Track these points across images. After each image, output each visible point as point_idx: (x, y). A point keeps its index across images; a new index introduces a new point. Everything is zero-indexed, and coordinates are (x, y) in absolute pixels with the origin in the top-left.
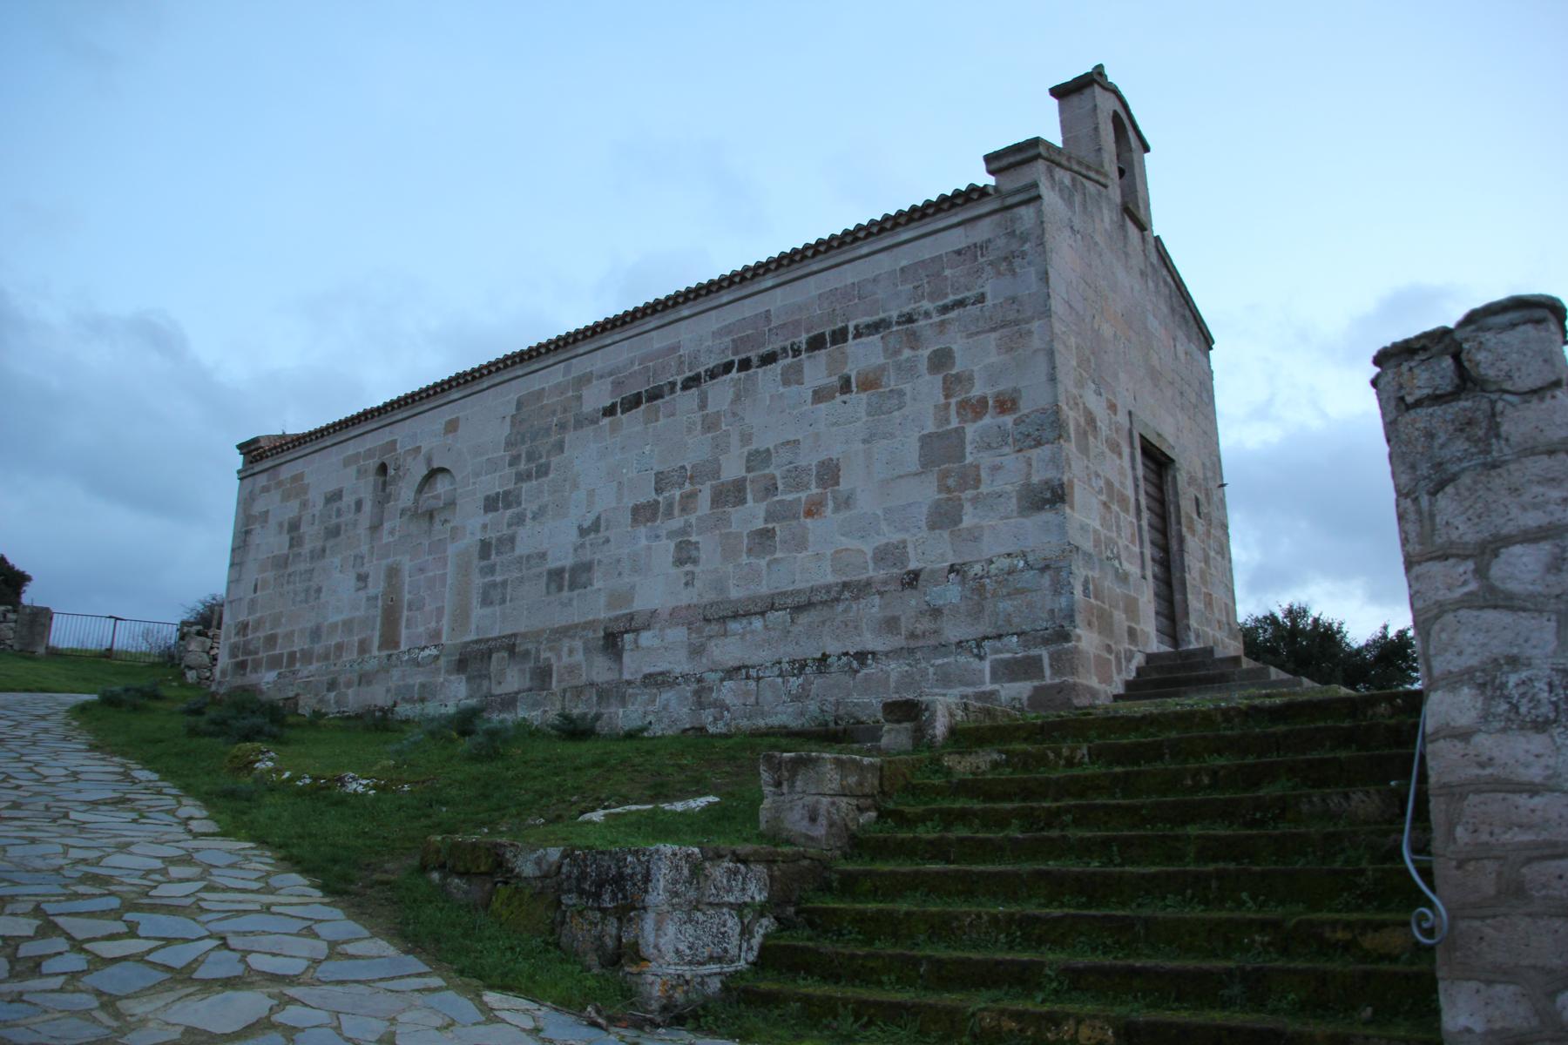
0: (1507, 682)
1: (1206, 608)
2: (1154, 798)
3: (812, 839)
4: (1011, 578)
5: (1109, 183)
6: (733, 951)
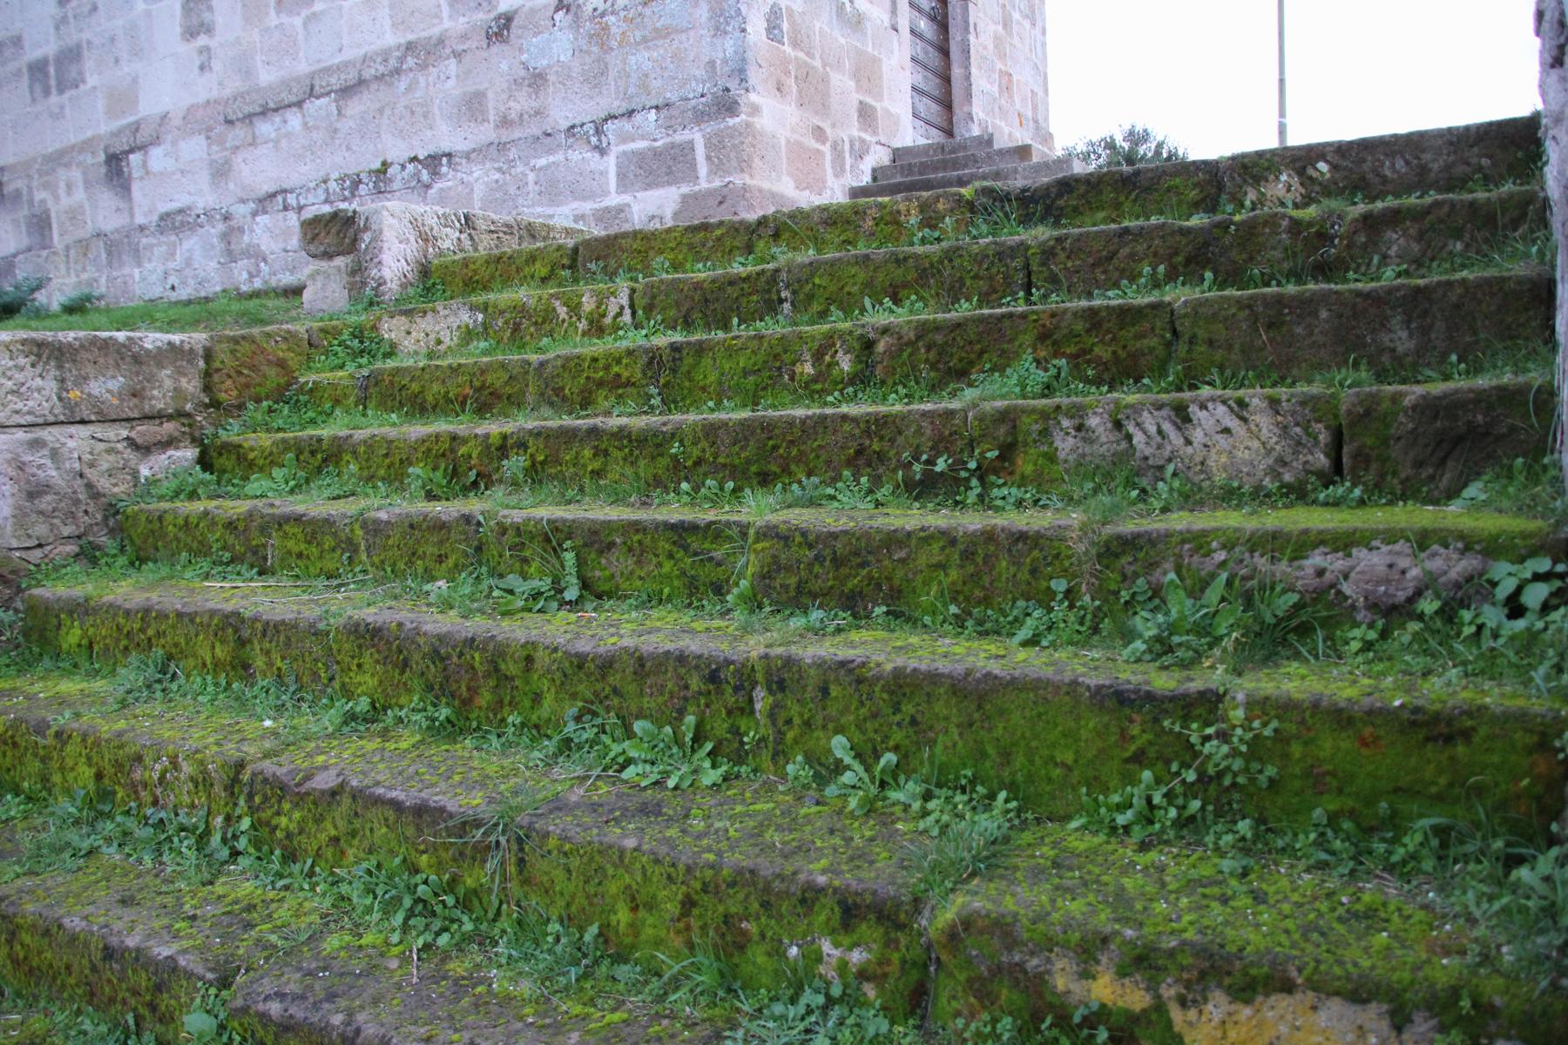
1: (1001, 92)
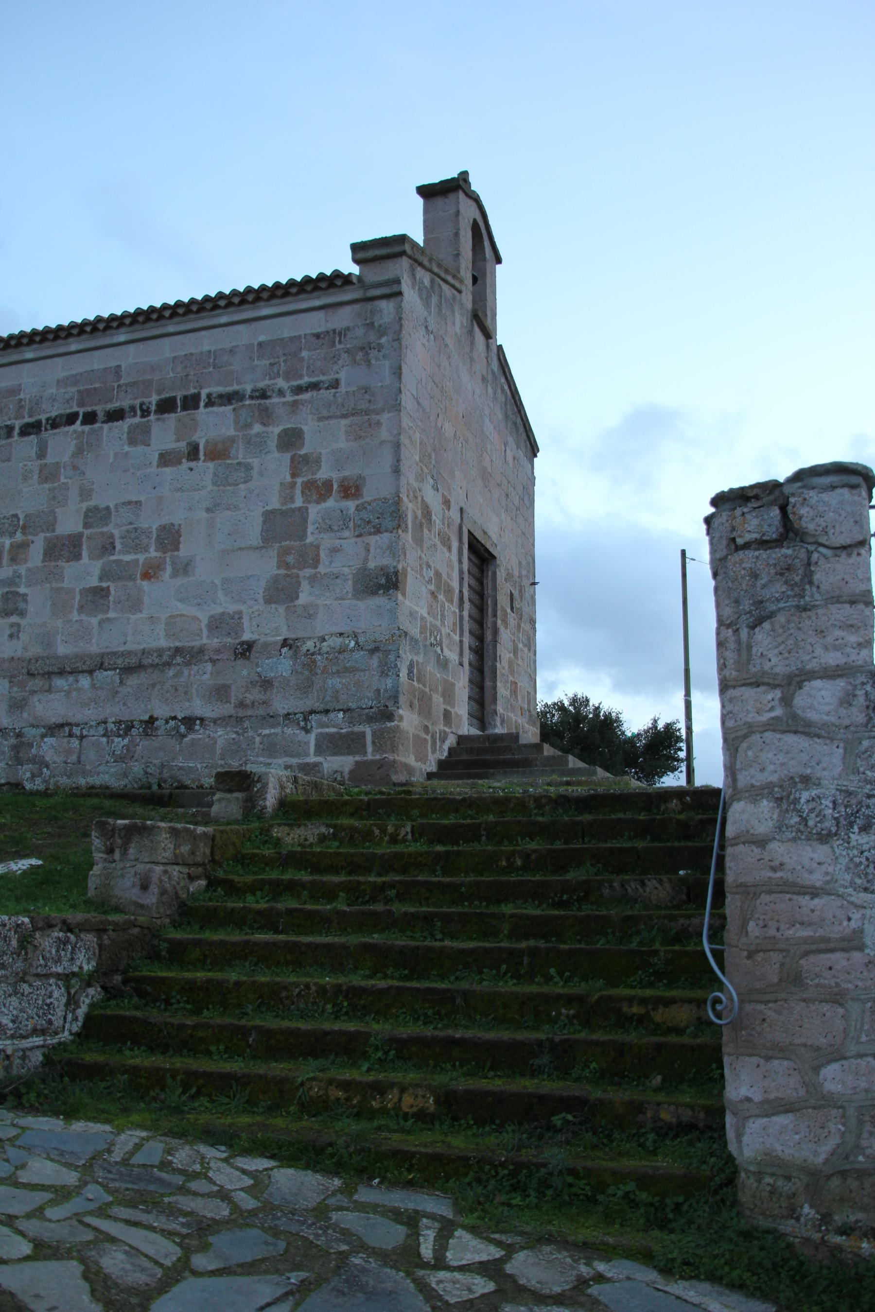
0: (800, 798)
1: (511, 694)
2: (471, 878)
3: (142, 906)
4: (341, 657)
5: (463, 289)
6: (58, 1022)
